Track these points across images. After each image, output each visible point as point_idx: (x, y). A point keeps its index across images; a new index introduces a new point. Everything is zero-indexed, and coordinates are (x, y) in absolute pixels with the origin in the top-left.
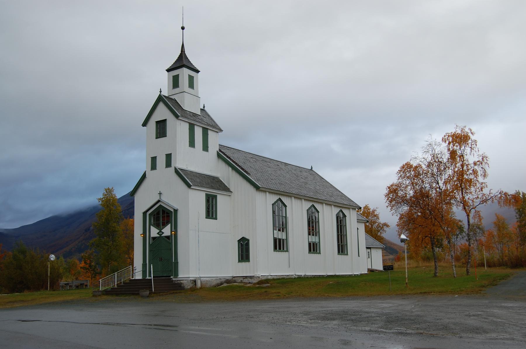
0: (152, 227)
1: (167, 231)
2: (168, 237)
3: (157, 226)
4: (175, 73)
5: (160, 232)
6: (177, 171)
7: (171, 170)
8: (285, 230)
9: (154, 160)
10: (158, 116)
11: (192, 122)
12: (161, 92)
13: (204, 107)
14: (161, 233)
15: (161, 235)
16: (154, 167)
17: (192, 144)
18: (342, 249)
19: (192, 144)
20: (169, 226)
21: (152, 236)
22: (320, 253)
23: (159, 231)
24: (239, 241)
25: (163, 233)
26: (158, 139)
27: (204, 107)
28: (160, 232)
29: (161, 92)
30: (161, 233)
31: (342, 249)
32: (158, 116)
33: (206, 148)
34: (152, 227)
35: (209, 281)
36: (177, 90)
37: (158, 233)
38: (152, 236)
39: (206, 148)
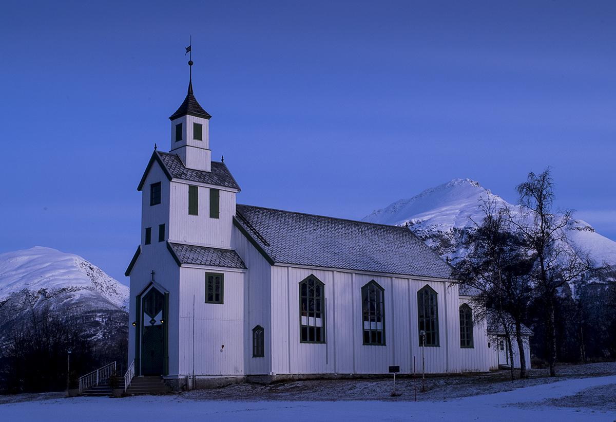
0: (145, 314)
1: (158, 319)
2: (159, 326)
3: (152, 314)
4: (178, 121)
5: (153, 320)
6: (169, 247)
7: (164, 243)
8: (321, 315)
9: (148, 232)
10: (151, 180)
11: (194, 183)
12: (156, 148)
13: (222, 160)
14: (153, 321)
15: (153, 324)
16: (148, 241)
17: (193, 209)
18: (467, 340)
19: (193, 209)
20: (161, 313)
21: (145, 325)
22: (384, 344)
23: (151, 319)
24: (254, 330)
25: (155, 321)
26: (153, 206)
27: (222, 160)
28: (153, 320)
29: (156, 148)
30: (153, 321)
31: (467, 340)
32: (151, 180)
33: (214, 212)
34: (145, 314)
35: (208, 380)
36: (180, 143)
37: (150, 322)
38: (145, 325)
39: (214, 212)
